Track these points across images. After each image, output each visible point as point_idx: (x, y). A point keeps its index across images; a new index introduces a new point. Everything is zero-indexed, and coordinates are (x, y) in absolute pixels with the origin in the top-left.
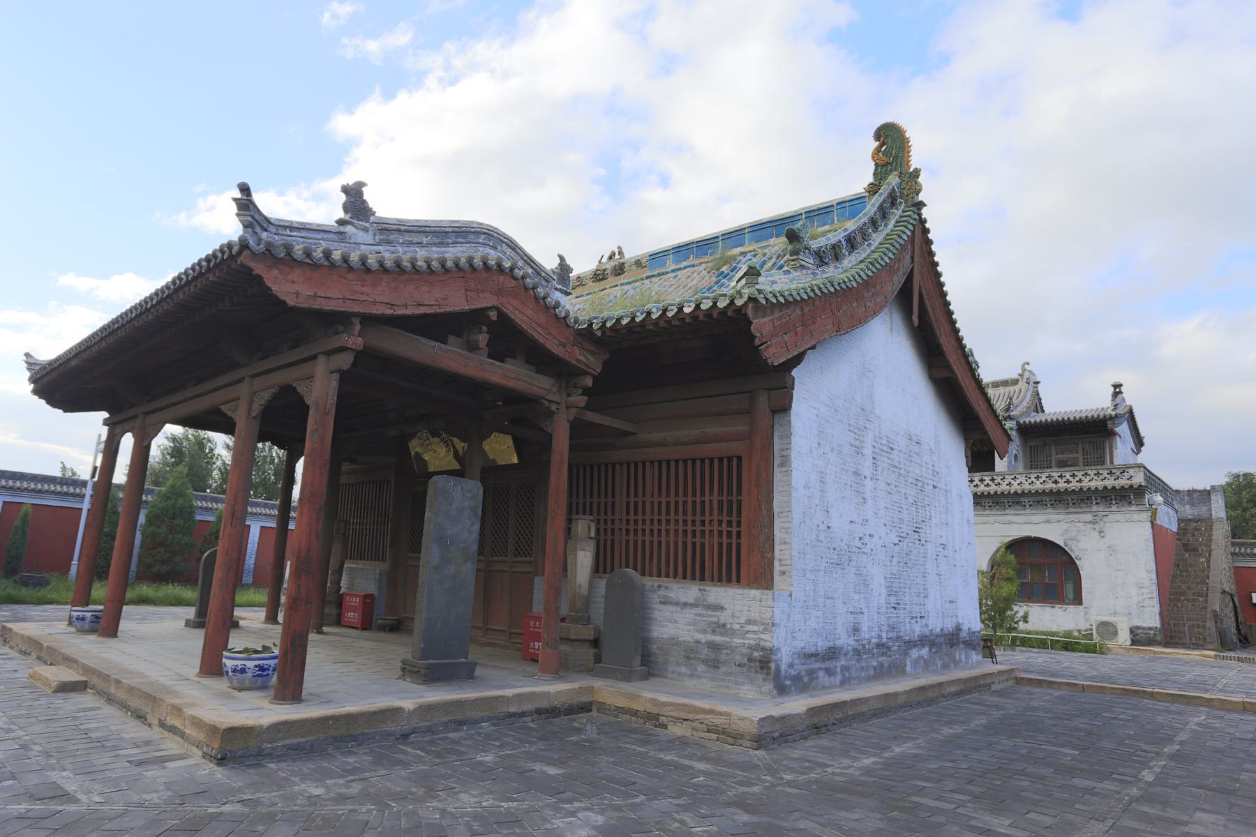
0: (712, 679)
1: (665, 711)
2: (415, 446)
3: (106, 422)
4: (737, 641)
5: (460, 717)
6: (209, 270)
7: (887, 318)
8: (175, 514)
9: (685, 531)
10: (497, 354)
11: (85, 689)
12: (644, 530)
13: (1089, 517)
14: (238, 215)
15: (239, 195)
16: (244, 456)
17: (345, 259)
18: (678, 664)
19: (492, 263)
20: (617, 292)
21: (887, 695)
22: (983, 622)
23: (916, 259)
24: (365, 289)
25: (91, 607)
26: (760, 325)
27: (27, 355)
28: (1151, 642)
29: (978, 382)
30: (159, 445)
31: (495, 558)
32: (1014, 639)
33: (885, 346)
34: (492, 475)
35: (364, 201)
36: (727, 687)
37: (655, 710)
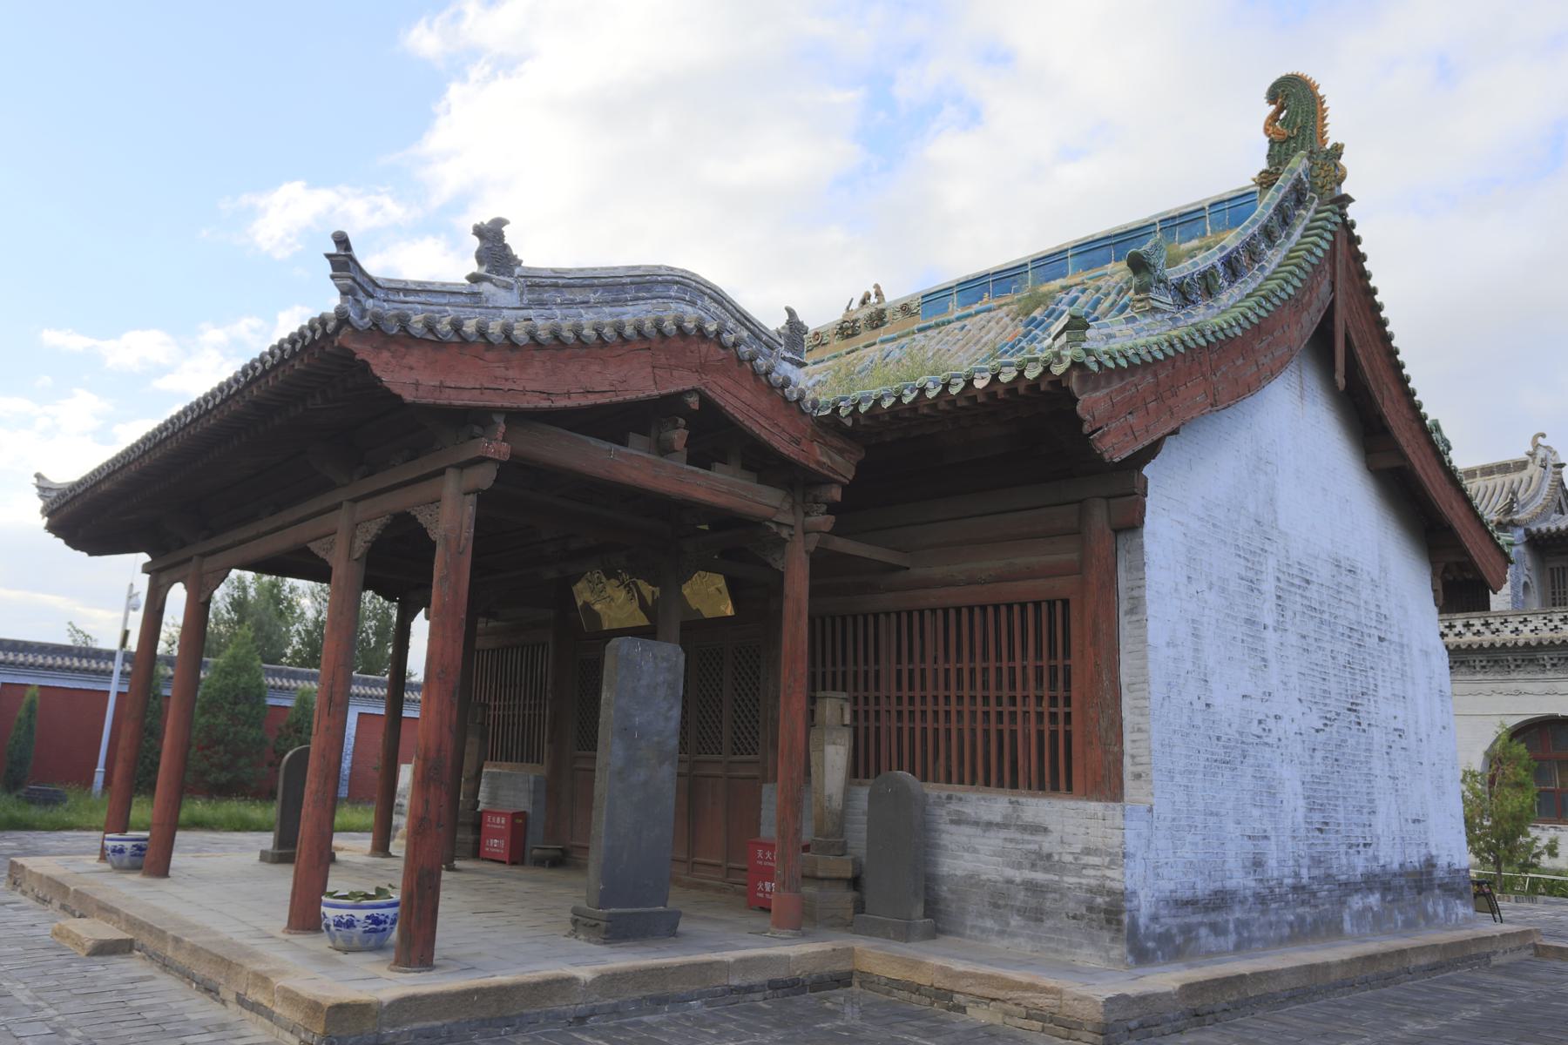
0: (1032, 938)
1: (962, 985)
2: (583, 593)
3: (147, 569)
4: (1070, 880)
5: (657, 993)
6: (294, 354)
7: (1294, 379)
8: (243, 697)
9: (986, 714)
10: (701, 457)
11: (130, 951)
12: (924, 713)
14: (332, 277)
15: (333, 249)
16: (345, 613)
17: (482, 332)
18: (981, 915)
19: (690, 325)
20: (875, 353)
21: (1311, 969)
22: (1477, 854)
23: (1338, 286)
24: (510, 374)
25: (131, 834)
26: (1091, 404)
27: (38, 476)
29: (1450, 473)
30: (221, 596)
31: (703, 757)
32: (1534, 884)
33: (1294, 424)
34: (698, 635)
35: (506, 247)
36: (1057, 951)
37: (947, 985)
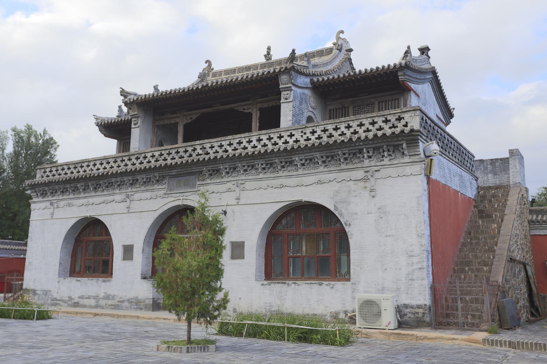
13: (360, 174)
28: (419, 324)
